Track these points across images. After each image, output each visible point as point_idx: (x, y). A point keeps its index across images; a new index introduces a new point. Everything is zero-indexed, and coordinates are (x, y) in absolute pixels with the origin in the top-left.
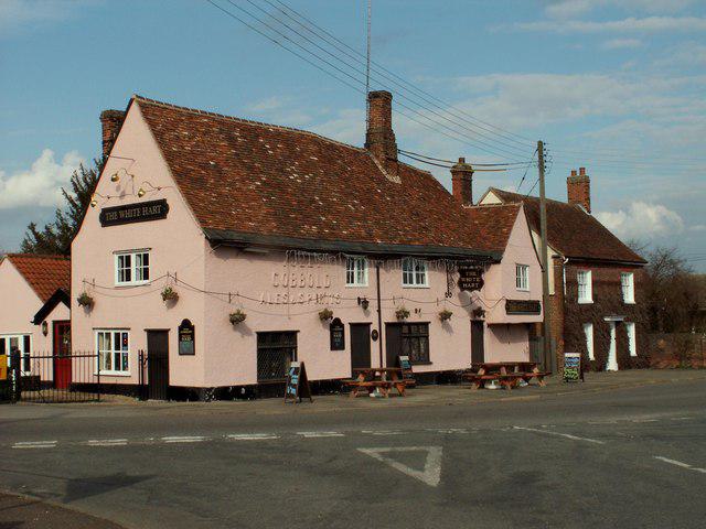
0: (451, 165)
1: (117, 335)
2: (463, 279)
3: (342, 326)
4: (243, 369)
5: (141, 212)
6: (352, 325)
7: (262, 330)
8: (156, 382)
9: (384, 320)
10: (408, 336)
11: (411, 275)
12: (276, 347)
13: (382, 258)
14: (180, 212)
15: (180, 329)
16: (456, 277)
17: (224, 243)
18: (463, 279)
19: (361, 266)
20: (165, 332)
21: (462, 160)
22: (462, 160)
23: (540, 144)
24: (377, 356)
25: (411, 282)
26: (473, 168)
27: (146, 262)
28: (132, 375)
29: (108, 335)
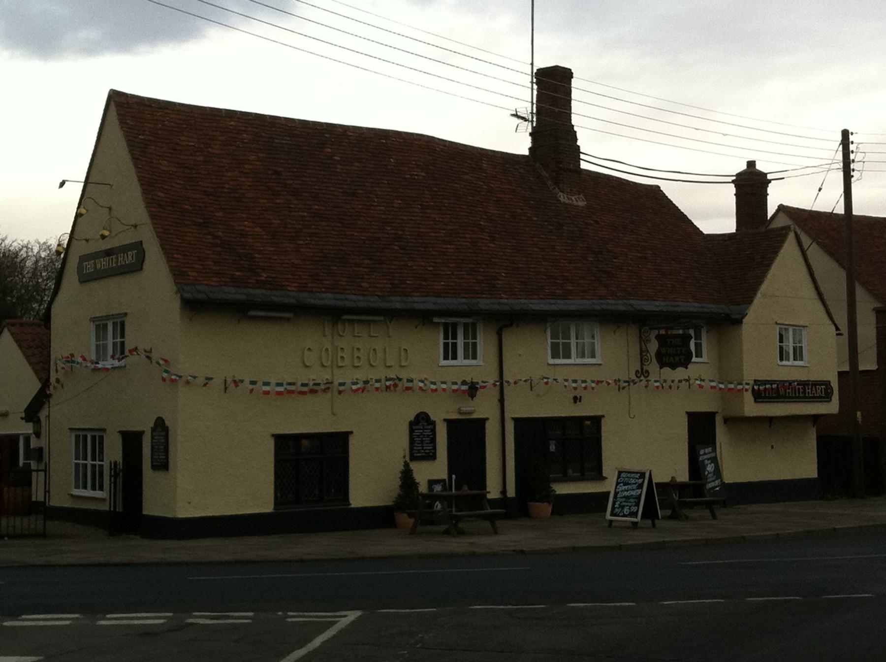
0: (730, 179)
1: (93, 437)
2: (664, 351)
3: (433, 423)
4: (256, 494)
5: (117, 262)
6: (450, 423)
7: (282, 432)
8: (128, 517)
9: (508, 415)
10: (563, 445)
11: (455, 345)
12: (311, 467)
13: (505, 321)
14: (156, 261)
15: (153, 430)
16: (653, 347)
17: (196, 306)
18: (664, 351)
19: (471, 332)
20: (139, 435)
21: (751, 164)
22: (751, 164)
23: (846, 134)
24: (499, 476)
25: (455, 357)
26: (769, 177)
27: (781, 348)
28: (99, 497)
29: (85, 437)
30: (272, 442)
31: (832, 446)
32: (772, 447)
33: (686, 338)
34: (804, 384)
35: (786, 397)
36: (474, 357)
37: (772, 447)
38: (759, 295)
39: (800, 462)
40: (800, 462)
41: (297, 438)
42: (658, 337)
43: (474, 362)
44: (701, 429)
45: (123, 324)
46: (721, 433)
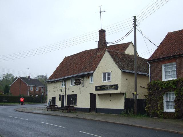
2: (76, 82)
23: (135, 17)
25: (106, 80)
30: (90, 94)
31: (128, 103)
32: (111, 101)
33: (80, 80)
34: (109, 86)
35: (103, 89)
36: (110, 80)
37: (111, 101)
38: (98, 67)
39: (120, 105)
40: (120, 105)
41: (69, 95)
42: (75, 79)
43: (110, 81)
44: (93, 97)
45: (110, 73)
46: (97, 98)
